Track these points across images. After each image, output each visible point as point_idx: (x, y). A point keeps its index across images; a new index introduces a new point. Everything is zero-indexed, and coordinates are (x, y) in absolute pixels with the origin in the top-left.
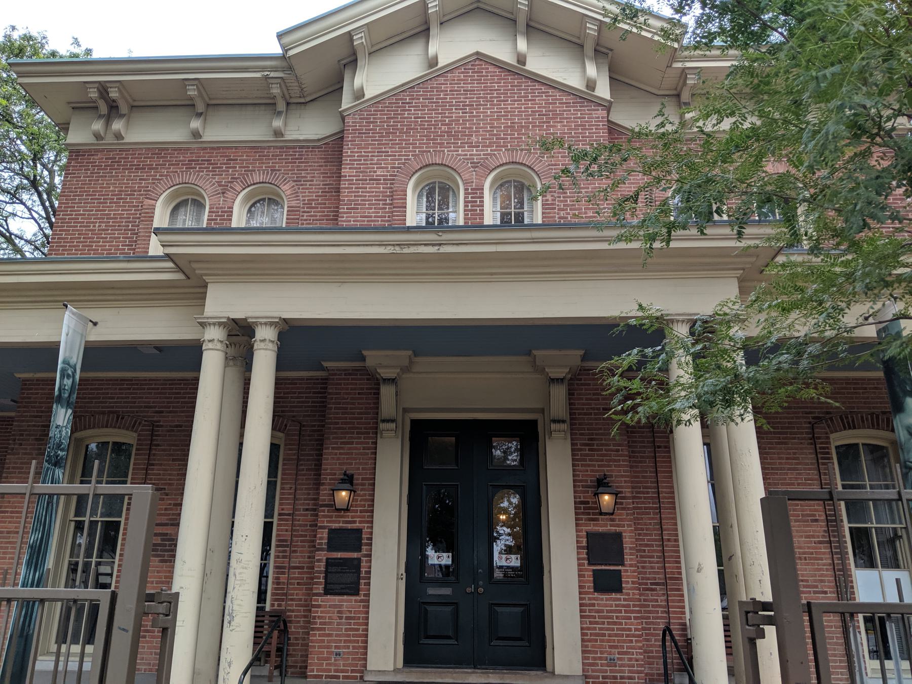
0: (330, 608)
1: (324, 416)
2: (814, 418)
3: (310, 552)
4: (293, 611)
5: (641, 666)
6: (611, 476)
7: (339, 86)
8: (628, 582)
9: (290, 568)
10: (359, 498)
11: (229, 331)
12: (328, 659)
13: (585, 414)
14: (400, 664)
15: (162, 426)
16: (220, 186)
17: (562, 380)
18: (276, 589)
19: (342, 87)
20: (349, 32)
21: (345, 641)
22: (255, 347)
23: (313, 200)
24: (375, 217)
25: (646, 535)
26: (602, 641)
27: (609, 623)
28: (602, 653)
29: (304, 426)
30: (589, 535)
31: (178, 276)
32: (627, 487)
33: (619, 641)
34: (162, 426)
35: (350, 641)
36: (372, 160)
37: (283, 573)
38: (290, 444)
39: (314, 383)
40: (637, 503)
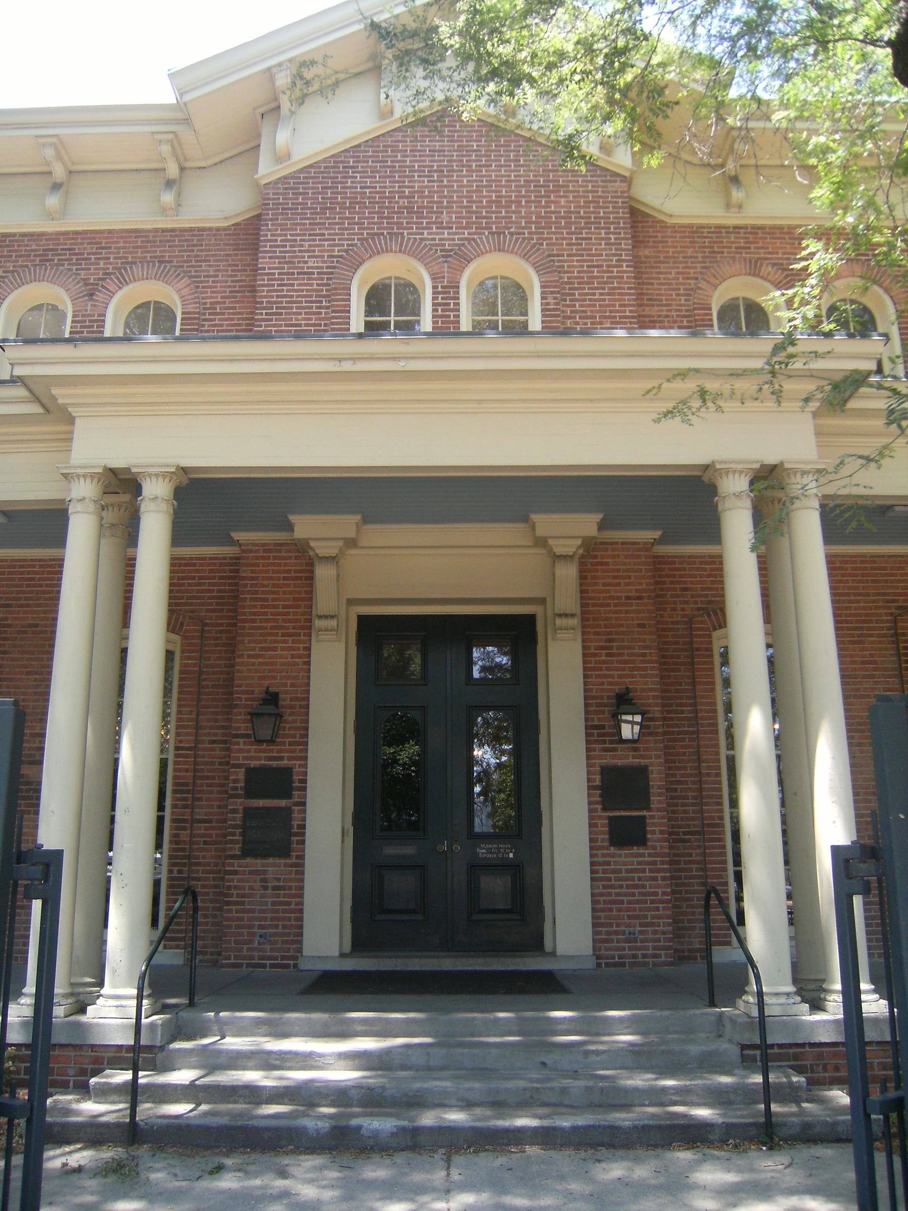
0: (250, 875)
1: (235, 611)
2: (898, 608)
3: (221, 800)
4: (199, 879)
5: (670, 940)
6: (635, 690)
7: (252, 144)
8: (654, 832)
9: (194, 821)
10: (287, 726)
11: (106, 487)
12: (250, 942)
13: (602, 605)
14: (347, 948)
15: (10, 626)
16: (86, 285)
17: (571, 557)
18: (174, 850)
19: (259, 146)
20: (269, 69)
21: (272, 919)
22: (143, 509)
23: (217, 303)
24: (306, 325)
25: (678, 768)
26: (619, 910)
27: (628, 887)
28: (618, 925)
29: (207, 625)
30: (606, 771)
31: (36, 409)
32: (657, 705)
33: (640, 909)
34: (10, 626)
35: (278, 919)
36: (301, 246)
37: (185, 829)
38: (188, 651)
39: (221, 565)
40: (668, 726)
